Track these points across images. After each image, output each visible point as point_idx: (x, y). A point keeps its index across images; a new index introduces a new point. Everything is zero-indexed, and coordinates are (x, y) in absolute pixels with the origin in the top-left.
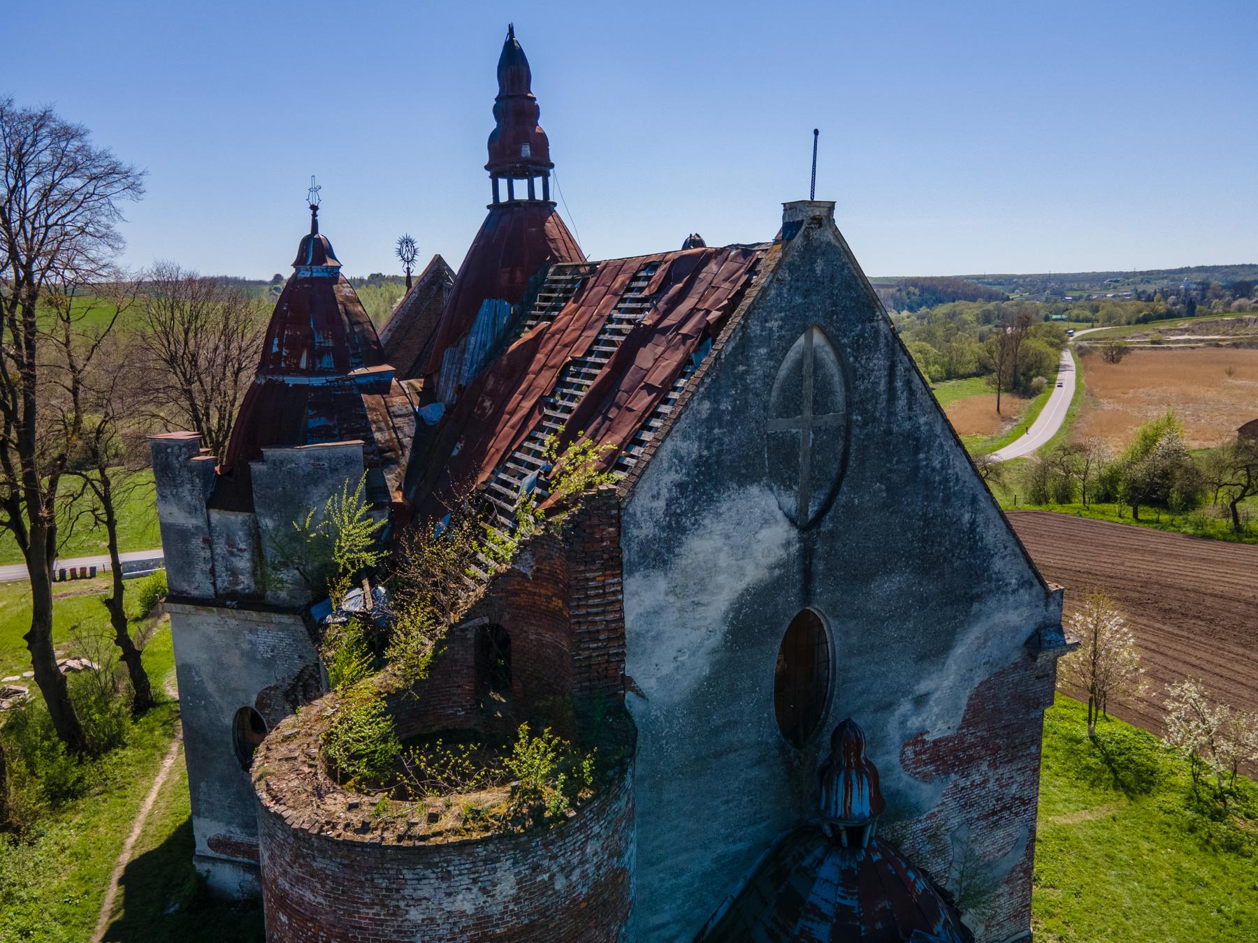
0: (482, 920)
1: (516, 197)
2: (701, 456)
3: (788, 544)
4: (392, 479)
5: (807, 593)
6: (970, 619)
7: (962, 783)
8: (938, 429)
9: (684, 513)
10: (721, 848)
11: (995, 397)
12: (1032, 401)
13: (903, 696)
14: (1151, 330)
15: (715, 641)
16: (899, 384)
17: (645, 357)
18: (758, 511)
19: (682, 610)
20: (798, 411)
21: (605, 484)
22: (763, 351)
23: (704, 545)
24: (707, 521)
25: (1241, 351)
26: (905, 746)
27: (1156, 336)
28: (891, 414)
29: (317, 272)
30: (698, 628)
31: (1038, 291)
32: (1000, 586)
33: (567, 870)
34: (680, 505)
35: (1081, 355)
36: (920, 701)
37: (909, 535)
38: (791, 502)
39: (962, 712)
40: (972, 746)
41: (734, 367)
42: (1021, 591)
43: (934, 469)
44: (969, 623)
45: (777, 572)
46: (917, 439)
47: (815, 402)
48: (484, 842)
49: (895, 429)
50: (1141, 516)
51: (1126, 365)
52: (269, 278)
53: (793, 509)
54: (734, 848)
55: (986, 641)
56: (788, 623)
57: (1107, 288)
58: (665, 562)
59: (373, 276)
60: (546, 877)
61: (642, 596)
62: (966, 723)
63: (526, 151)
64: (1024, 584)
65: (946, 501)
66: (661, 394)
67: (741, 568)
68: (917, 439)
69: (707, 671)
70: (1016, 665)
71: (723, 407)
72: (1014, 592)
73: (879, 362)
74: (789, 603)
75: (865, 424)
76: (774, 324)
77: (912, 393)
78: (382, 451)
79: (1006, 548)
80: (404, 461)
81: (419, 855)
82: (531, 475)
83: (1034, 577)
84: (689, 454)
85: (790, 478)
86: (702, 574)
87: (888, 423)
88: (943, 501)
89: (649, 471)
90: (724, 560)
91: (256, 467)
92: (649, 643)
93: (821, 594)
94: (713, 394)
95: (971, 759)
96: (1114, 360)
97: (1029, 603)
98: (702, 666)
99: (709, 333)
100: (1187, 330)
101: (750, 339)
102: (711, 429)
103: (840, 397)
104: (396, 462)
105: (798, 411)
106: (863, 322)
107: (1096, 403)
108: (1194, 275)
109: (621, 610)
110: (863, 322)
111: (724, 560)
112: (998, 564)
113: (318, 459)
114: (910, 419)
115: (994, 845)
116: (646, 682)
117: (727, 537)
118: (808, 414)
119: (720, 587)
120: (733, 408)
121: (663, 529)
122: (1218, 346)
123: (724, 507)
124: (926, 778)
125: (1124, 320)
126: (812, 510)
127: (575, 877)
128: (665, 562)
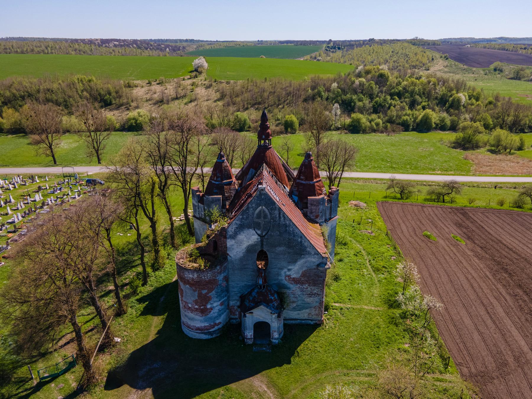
3: (258, 239)
4: (227, 203)
6: (301, 258)
8: (291, 224)
10: (246, 283)
20: (260, 218)
23: (242, 237)
29: (220, 161)
32: (309, 253)
36: (289, 270)
65: (294, 236)
73: (277, 212)
74: (259, 248)
77: (284, 217)
90: (245, 239)
94: (242, 215)
95: (303, 283)
103: (269, 217)
105: (260, 218)
111: (245, 239)
112: (308, 249)
124: (291, 283)
126: (264, 234)
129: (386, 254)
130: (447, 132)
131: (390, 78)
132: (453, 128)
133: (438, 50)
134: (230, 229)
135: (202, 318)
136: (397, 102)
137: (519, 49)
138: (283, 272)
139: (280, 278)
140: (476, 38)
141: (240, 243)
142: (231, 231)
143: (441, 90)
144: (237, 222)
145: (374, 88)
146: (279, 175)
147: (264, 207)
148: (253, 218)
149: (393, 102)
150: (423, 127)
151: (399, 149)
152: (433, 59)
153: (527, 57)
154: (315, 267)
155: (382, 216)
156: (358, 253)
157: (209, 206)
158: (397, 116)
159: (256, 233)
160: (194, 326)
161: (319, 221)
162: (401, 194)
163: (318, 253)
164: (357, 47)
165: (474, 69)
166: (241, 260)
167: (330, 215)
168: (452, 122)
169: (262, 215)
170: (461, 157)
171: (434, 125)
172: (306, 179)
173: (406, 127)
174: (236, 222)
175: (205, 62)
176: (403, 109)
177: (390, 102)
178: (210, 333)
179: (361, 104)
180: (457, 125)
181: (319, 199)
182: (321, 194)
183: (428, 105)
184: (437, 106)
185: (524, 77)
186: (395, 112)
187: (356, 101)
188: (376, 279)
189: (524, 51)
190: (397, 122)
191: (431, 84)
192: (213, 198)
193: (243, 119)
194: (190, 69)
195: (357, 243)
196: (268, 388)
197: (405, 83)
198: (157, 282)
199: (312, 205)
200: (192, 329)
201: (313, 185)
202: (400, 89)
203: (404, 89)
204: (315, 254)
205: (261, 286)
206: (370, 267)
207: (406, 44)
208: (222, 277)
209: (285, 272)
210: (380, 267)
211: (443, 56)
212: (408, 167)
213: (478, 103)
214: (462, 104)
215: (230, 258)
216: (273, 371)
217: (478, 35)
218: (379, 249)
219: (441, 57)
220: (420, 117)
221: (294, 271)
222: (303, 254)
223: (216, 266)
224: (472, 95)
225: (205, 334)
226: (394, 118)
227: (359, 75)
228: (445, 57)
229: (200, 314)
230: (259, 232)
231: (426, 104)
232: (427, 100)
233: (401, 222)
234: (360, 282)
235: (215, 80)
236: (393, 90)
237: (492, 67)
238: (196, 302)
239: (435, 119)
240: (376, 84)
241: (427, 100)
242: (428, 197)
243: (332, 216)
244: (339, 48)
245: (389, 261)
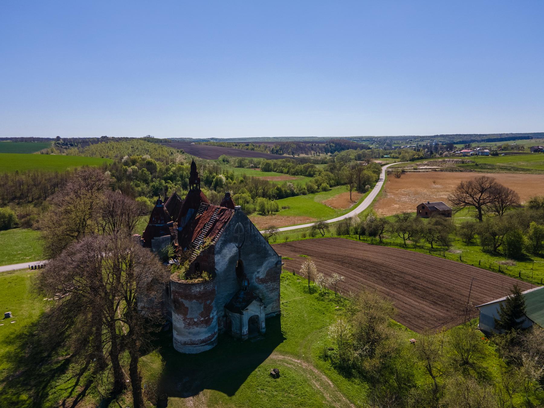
0: (200, 292)
5: (240, 256)
11: (349, 193)
12: (363, 195)
14: (414, 164)
17: (218, 224)
21: (212, 243)
23: (225, 251)
25: (443, 173)
27: (415, 167)
28: (251, 232)
29: (160, 206)
31: (382, 144)
32: (270, 255)
35: (388, 175)
36: (258, 272)
38: (237, 245)
50: (361, 239)
51: (403, 179)
57: (407, 143)
61: (217, 258)
62: (266, 276)
63: (196, 181)
66: (220, 230)
73: (249, 225)
80: (177, 237)
81: (193, 284)
82: (201, 241)
83: (276, 254)
91: (152, 240)
96: (398, 177)
98: (225, 267)
99: (226, 223)
100: (426, 164)
107: (386, 195)
108: (439, 138)
112: (270, 252)
115: (272, 295)
116: (218, 269)
122: (436, 171)
124: (260, 284)
125: (408, 159)
134: (217, 246)
135: (206, 329)
138: (254, 276)
152: (172, 153)
154: (274, 266)
160: (198, 341)
165: (208, 161)
178: (212, 343)
179: (140, 189)
185: (245, 166)
189: (237, 148)
192: (163, 239)
193: (7, 215)
196: (283, 355)
200: (197, 344)
202: (171, 173)
203: (174, 173)
216: (278, 347)
225: (208, 344)
228: (181, 152)
229: (205, 326)
237: (221, 158)
238: (202, 315)
240: (148, 170)
244: (72, 145)
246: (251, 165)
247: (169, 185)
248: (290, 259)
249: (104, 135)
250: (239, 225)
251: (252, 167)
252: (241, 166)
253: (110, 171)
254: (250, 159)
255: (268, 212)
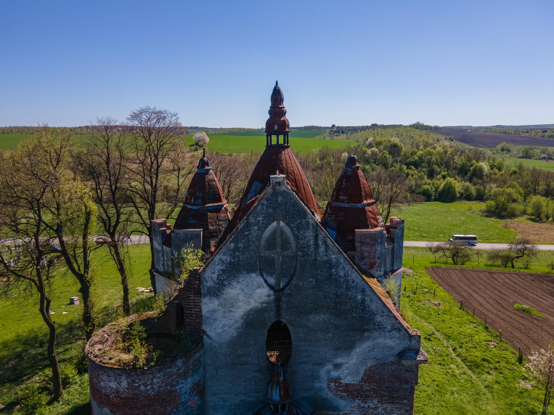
1: (280, 143)
2: (231, 261)
3: (269, 296)
7: (363, 405)
9: (225, 280)
10: (243, 397)
13: (328, 362)
15: (239, 324)
16: (320, 242)
18: (255, 283)
19: (224, 312)
22: (256, 228)
23: (234, 291)
24: (234, 284)
26: (330, 382)
28: (317, 253)
29: (202, 171)
30: (231, 319)
32: (380, 328)
33: (146, 385)
34: (223, 277)
36: (337, 366)
37: (328, 300)
39: (361, 375)
40: (367, 391)
41: (244, 232)
42: (393, 332)
43: (340, 276)
44: (363, 340)
45: (264, 305)
46: (331, 264)
47: (282, 246)
48: (117, 369)
49: (319, 259)
52: (330, 126)
53: (274, 283)
54: (248, 399)
55: (373, 349)
56: (270, 324)
58: (217, 295)
59: (373, 125)
60: (137, 385)
64: (394, 329)
65: (348, 289)
67: (249, 301)
68: (331, 264)
69: (235, 334)
70: (392, 363)
71: (239, 246)
72: (389, 331)
74: (271, 318)
75: (304, 256)
76: (260, 219)
78: (211, 233)
79: (383, 312)
84: (226, 260)
85: (272, 272)
86: (232, 301)
87: (315, 256)
88: (346, 289)
89: (210, 264)
90: (241, 297)
92: (212, 321)
93: (285, 316)
94: (236, 241)
95: (367, 396)
97: (399, 338)
101: (250, 224)
102: (234, 253)
103: (293, 245)
104: (217, 237)
106: (301, 219)
109: (200, 308)
110: (301, 219)
112: (378, 318)
113: (187, 234)
114: (326, 256)
116: (212, 334)
117: (243, 290)
118: (279, 250)
119: (240, 307)
120: (244, 246)
121: (216, 284)
123: (241, 280)
124: (342, 397)
126: (282, 285)
127: (149, 387)
128: (217, 295)
129: (477, 337)
130: (474, 202)
131: (404, 148)
132: (480, 197)
133: (441, 133)
134: (208, 274)
136: (413, 171)
137: (521, 133)
138: (323, 372)
139: (317, 385)
140: (473, 126)
141: (231, 305)
142: (211, 276)
143: (459, 160)
144: (224, 258)
145: (388, 158)
146: (303, 191)
147: (282, 224)
148: (258, 247)
149: (410, 172)
150: (447, 196)
151: (425, 218)
152: (438, 140)
153: (532, 138)
154: (392, 359)
155: (440, 285)
156: (430, 335)
157: (179, 249)
158: (416, 185)
159: (266, 281)
161: (377, 274)
162: (453, 258)
163: (399, 328)
164: (361, 131)
165: (482, 149)
166: (233, 343)
167: (392, 265)
168: (478, 191)
169: (279, 240)
170: (500, 226)
171: (458, 195)
172: (350, 200)
173: (427, 197)
174: (222, 257)
175: (207, 136)
176: (421, 178)
177: (406, 171)
180: (484, 195)
181: (375, 233)
182: (376, 226)
183: (448, 174)
184: (458, 175)
185: (534, 156)
186: (414, 181)
187: (370, 170)
188: (480, 383)
189: (527, 135)
190: (417, 191)
191: (448, 153)
194: (190, 143)
195: (423, 321)
197: (421, 152)
198: (80, 394)
199: (362, 243)
201: (363, 211)
202: (417, 158)
203: (420, 158)
204: (394, 329)
205: (276, 407)
206: (459, 360)
207: (409, 128)
208: (189, 386)
209: (329, 372)
210: (479, 360)
211: (448, 138)
212: (441, 236)
213: (501, 173)
214: (485, 173)
215: (209, 341)
217: (475, 125)
218: (461, 330)
219: (446, 139)
220: (442, 186)
221: (347, 368)
222: (368, 330)
223: (174, 359)
224: (493, 165)
226: (414, 187)
227: (370, 146)
228: (450, 139)
230: (272, 281)
231: (446, 173)
232: (446, 169)
233: (470, 291)
234: (454, 389)
235: (217, 153)
236: (408, 160)
237: (499, 147)
239: (459, 188)
240: (390, 153)
241: (446, 169)
242: (490, 263)
243: (395, 268)
244: (343, 133)
245: (487, 349)
246: (543, 155)
247: (410, 172)
248: (535, 313)
249: (374, 123)
250: (278, 228)
251: (544, 158)
252: (527, 156)
253: (348, 153)
254: (542, 148)
255: (547, 217)
